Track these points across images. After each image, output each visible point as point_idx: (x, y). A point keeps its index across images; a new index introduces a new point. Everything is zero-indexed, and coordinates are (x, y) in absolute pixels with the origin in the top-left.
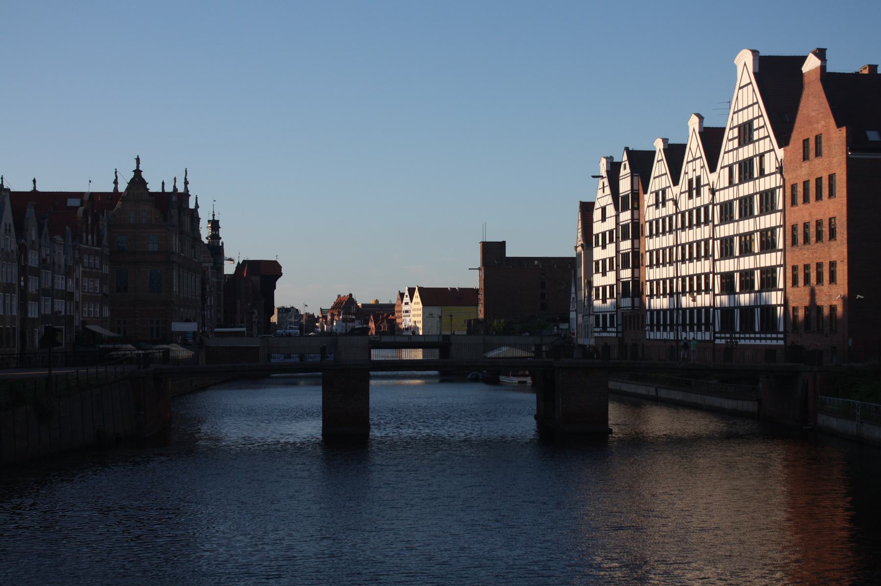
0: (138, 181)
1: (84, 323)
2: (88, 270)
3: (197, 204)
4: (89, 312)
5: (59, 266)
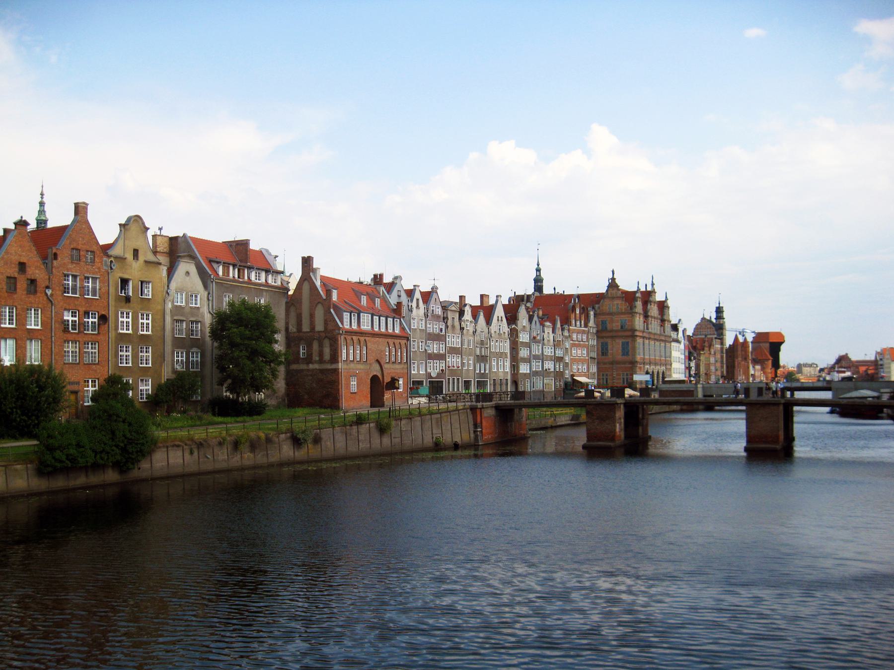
0: (613, 284)
1: (572, 376)
2: (577, 342)
3: (666, 297)
4: (578, 369)
5: (549, 341)
